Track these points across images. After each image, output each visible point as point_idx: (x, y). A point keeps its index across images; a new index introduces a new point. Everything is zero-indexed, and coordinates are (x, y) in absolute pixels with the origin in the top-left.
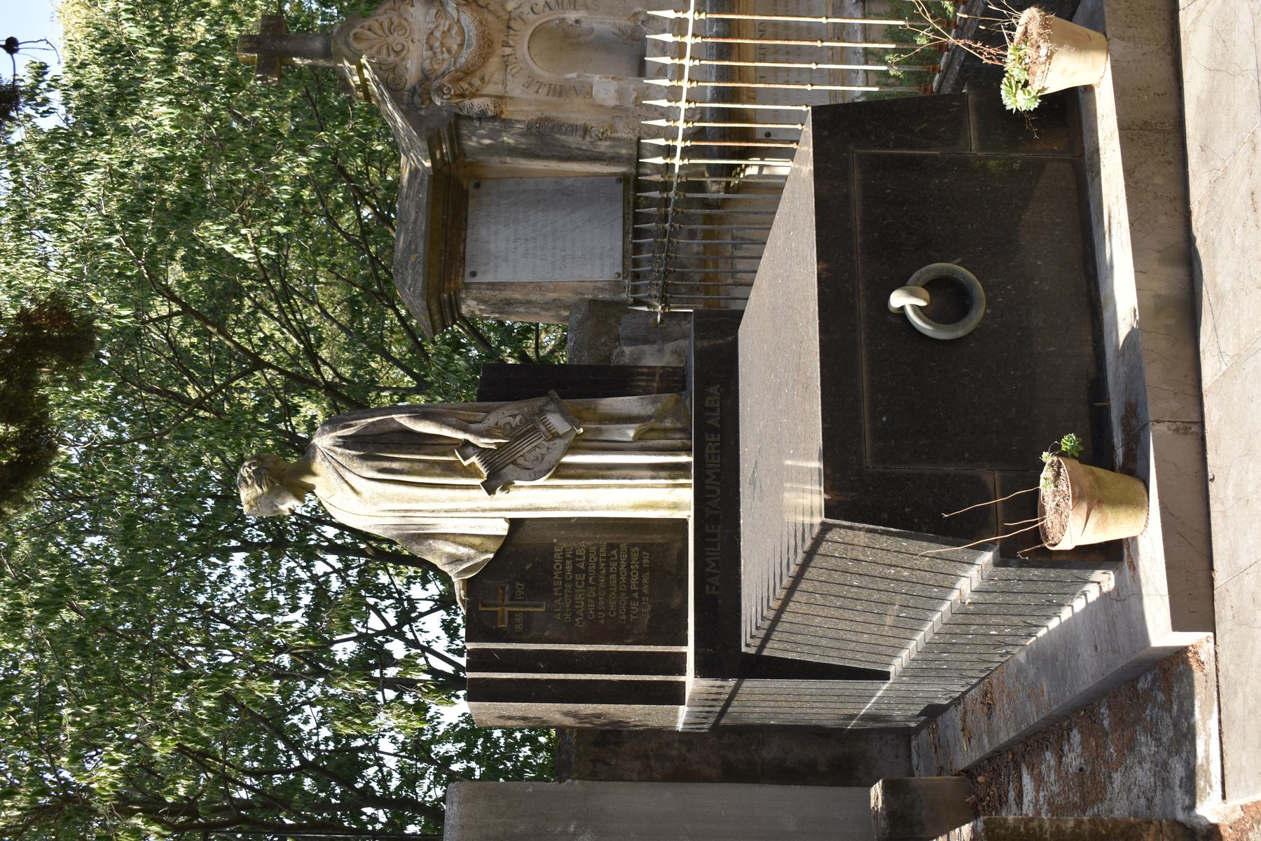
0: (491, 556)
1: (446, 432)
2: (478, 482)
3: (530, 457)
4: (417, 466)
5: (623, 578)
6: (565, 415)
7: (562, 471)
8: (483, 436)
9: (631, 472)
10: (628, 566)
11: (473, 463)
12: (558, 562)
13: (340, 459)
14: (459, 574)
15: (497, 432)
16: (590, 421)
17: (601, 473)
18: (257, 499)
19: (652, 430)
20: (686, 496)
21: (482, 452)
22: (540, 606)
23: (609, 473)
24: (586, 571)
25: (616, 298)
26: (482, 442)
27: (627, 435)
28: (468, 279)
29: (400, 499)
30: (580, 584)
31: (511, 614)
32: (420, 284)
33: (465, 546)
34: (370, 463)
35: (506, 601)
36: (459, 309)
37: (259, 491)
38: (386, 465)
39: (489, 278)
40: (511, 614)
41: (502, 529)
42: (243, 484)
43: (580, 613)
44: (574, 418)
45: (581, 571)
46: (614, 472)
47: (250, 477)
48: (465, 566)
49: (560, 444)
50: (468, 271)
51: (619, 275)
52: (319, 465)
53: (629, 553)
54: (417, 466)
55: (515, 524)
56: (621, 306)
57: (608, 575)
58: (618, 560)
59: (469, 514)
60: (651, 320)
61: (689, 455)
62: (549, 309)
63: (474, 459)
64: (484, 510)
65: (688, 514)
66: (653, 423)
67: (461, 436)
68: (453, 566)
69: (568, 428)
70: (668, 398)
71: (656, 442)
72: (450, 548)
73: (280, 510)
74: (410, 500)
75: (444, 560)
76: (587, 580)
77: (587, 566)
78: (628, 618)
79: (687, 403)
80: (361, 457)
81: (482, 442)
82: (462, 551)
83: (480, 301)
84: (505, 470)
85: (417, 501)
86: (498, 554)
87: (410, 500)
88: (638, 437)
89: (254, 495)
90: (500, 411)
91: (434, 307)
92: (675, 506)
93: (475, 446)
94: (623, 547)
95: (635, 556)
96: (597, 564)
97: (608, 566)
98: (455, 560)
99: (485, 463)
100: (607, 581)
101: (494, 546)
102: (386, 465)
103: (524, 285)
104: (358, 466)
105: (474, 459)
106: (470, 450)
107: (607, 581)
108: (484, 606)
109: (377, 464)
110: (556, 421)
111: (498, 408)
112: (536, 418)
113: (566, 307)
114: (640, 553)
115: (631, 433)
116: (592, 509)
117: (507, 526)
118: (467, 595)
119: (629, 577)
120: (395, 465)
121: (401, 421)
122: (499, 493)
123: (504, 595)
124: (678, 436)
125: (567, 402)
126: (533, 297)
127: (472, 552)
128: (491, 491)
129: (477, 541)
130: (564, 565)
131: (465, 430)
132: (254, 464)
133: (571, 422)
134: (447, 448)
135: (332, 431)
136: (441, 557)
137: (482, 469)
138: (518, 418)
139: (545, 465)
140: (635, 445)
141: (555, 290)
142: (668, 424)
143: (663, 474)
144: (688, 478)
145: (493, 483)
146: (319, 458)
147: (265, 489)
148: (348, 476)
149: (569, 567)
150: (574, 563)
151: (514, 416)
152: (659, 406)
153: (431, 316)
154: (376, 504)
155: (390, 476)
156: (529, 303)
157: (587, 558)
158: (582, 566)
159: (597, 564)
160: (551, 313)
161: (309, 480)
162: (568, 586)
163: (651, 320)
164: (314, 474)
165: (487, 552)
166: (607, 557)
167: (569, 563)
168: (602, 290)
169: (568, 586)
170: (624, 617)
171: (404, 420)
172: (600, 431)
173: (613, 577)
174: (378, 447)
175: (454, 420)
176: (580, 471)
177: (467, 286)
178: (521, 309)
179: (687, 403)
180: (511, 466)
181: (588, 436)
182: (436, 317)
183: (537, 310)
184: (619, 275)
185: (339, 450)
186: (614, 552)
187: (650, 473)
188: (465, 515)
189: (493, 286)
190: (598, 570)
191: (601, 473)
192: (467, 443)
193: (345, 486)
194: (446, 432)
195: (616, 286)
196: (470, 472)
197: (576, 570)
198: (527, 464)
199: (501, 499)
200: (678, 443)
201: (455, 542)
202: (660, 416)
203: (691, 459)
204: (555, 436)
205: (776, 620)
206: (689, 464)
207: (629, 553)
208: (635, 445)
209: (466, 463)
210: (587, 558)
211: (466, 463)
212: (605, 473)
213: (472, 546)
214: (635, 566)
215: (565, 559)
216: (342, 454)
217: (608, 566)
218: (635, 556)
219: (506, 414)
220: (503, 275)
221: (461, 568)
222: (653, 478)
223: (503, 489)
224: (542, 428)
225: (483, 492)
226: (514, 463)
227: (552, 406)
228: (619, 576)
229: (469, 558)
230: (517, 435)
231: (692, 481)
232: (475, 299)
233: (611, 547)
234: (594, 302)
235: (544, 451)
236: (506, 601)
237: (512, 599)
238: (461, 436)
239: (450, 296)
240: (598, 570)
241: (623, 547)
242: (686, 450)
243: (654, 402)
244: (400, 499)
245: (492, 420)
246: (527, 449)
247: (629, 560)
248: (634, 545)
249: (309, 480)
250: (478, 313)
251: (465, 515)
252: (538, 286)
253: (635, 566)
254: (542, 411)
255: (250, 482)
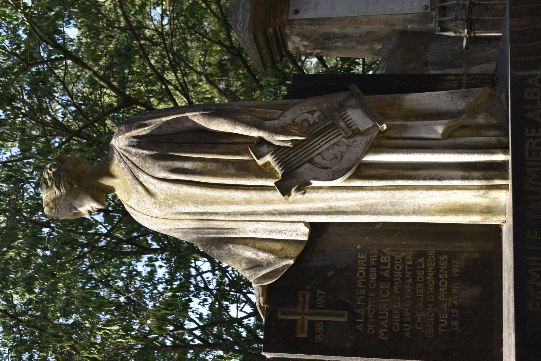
0: (291, 262)
1: (240, 130)
2: (271, 183)
3: (329, 155)
4: (210, 166)
5: (431, 288)
6: (368, 112)
7: (364, 171)
8: (278, 133)
9: (440, 173)
10: (436, 275)
11: (268, 163)
12: (361, 270)
13: (134, 159)
14: (259, 280)
15: (294, 129)
16: (395, 118)
17: (406, 173)
18: (55, 201)
19: (463, 127)
20: (504, 198)
21: (277, 150)
22: (343, 316)
23: (415, 173)
24: (391, 280)
25: (424, 28)
26: (278, 140)
27: (436, 132)
28: (292, 16)
29: (195, 201)
30: (384, 293)
31: (312, 324)
32: (247, 20)
33: (264, 250)
34: (162, 163)
35: (307, 310)
36: (286, 46)
37: (58, 192)
38: (179, 164)
39: (310, 14)
40: (312, 324)
41: (301, 233)
42: (44, 186)
43: (385, 324)
44: (378, 115)
45: (386, 280)
46: (420, 173)
47: (50, 179)
48: (264, 272)
49: (361, 141)
50: (292, 9)
51: (427, 7)
52: (117, 167)
53: (437, 261)
54: (210, 166)
55: (316, 229)
56: (430, 37)
57: (414, 284)
58: (426, 269)
59: (266, 218)
60: (457, 47)
61: (506, 152)
62: (363, 43)
63: (268, 158)
64: (282, 214)
65: (505, 221)
66: (464, 120)
67: (255, 133)
68: (252, 272)
69: (369, 124)
70: (480, 93)
71: (468, 139)
72: (249, 253)
73: (79, 213)
74: (205, 202)
75: (244, 265)
76: (392, 288)
77: (392, 274)
78: (436, 331)
79: (503, 97)
80: (153, 157)
81: (278, 140)
82: (262, 256)
83: (304, 36)
84: (301, 169)
85: (212, 203)
86: (299, 260)
87: (205, 202)
88: (447, 134)
89: (53, 196)
90: (297, 108)
91: (261, 40)
92: (489, 210)
93: (270, 144)
94: (431, 254)
95: (444, 265)
96: (403, 272)
97: (414, 275)
98: (255, 265)
99: (280, 161)
100: (414, 291)
101: (295, 252)
102: (179, 164)
103: (340, 20)
104: (148, 165)
105: (268, 158)
106: (265, 148)
107: (414, 291)
108: (284, 313)
109: (169, 163)
110: (358, 118)
111: (296, 104)
112: (336, 114)
113: (380, 40)
114: (449, 261)
115: (440, 130)
116: (397, 213)
117: (307, 230)
118: (266, 301)
119: (437, 287)
120: (188, 165)
121: (195, 120)
122: (295, 195)
123: (304, 302)
124: (492, 133)
125: (371, 99)
126: (350, 30)
127: (272, 257)
128: (285, 192)
129: (277, 246)
130: (368, 272)
131: (260, 127)
132: (54, 166)
133: (373, 118)
134: (242, 147)
135: (127, 131)
136: (240, 262)
137: (277, 168)
138: (316, 115)
139: (345, 164)
140: (444, 142)
141: (368, 23)
142: (481, 120)
143: (475, 174)
144: (505, 178)
145: (288, 183)
146: (116, 161)
147: (63, 191)
148: (143, 177)
149: (373, 275)
150: (378, 271)
151: (312, 113)
152: (471, 100)
153: (259, 49)
154: (171, 206)
155: (183, 176)
156: (346, 36)
157: (393, 265)
158: (387, 274)
159: (403, 272)
160: (366, 47)
161: (108, 182)
162: (371, 294)
163: (457, 47)
164: (112, 176)
165: (287, 257)
166: (413, 265)
167: (372, 270)
168: (411, 21)
169: (371, 294)
170: (432, 330)
171: (197, 118)
172: (405, 128)
173: (419, 286)
174: (171, 146)
175: (248, 117)
176: (383, 171)
177: (291, 22)
178: (340, 44)
179: (503, 97)
180: (308, 165)
181: (392, 134)
182: (265, 51)
183: (353, 44)
184: (427, 7)
185: (134, 150)
186: (421, 260)
187: (461, 173)
188: (266, 219)
189: (313, 21)
190: (403, 278)
191: (406, 173)
192: (261, 140)
193: (139, 187)
194: (240, 130)
195: (425, 17)
196: (264, 172)
197: (380, 278)
198: (326, 163)
199: (298, 201)
200: (493, 140)
201: (254, 247)
202: (472, 111)
203: (509, 158)
204: (357, 133)
205: (179, 133)
206: (505, 163)
207: (437, 261)
208: (444, 142)
209: (260, 162)
210: (393, 265)
211: (260, 162)
212: (410, 173)
213: (271, 251)
214: (443, 275)
215: (368, 267)
216: (136, 155)
217: (414, 275)
218: (444, 265)
219: (303, 111)
220: (323, 12)
221: (261, 274)
222: (464, 178)
223: (298, 190)
224: (342, 124)
225: (278, 195)
226: (311, 161)
227: (353, 102)
228: (426, 285)
229: (269, 264)
230: (314, 132)
231: (509, 182)
232: (298, 35)
233: (421, 254)
234: (404, 33)
235: (343, 149)
236: (307, 310)
237: (312, 307)
238: (255, 133)
239: (275, 30)
240: (403, 278)
241: (431, 254)
242: (504, 149)
243: (465, 96)
244: (195, 201)
245: (288, 117)
246: (325, 147)
247: (437, 269)
248: (442, 253)
249: (108, 182)
250: (302, 49)
251: (266, 219)
252: (354, 20)
253: (443, 275)
254: (342, 107)
255: (50, 183)
